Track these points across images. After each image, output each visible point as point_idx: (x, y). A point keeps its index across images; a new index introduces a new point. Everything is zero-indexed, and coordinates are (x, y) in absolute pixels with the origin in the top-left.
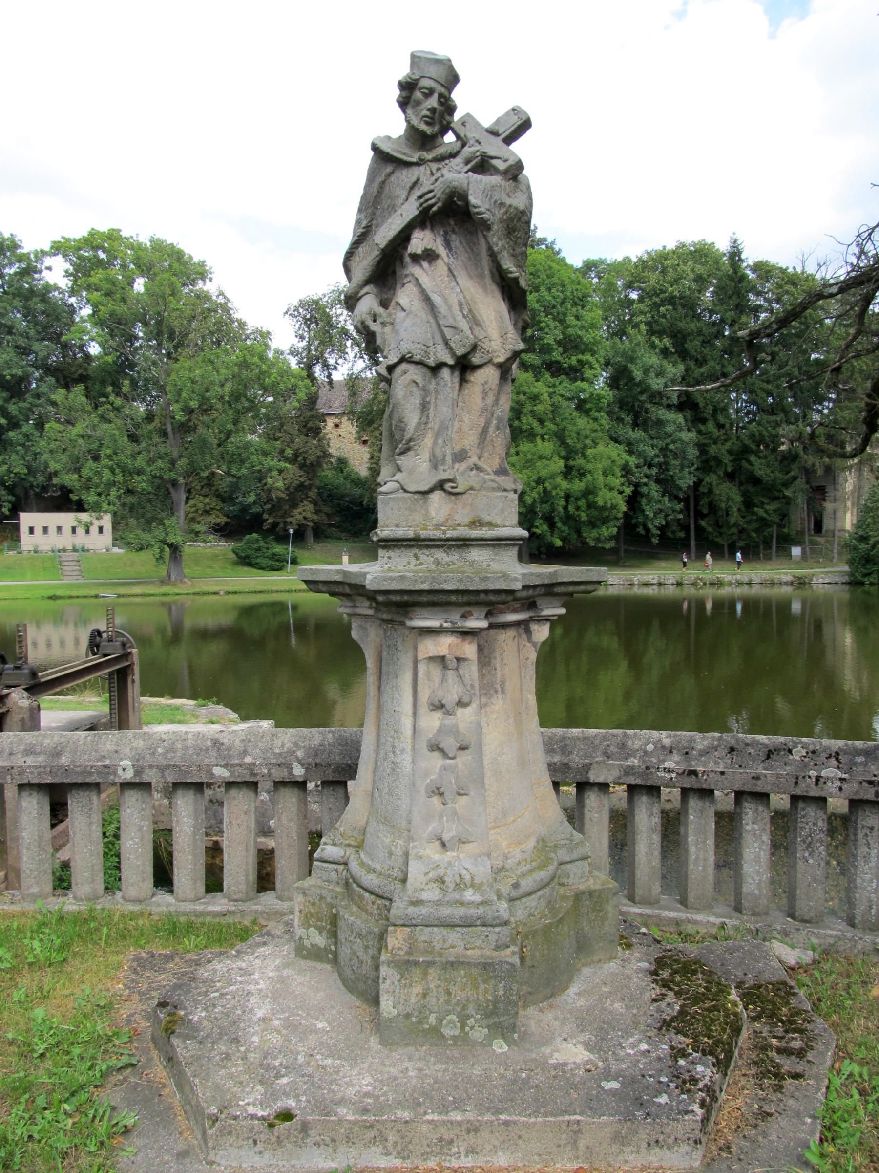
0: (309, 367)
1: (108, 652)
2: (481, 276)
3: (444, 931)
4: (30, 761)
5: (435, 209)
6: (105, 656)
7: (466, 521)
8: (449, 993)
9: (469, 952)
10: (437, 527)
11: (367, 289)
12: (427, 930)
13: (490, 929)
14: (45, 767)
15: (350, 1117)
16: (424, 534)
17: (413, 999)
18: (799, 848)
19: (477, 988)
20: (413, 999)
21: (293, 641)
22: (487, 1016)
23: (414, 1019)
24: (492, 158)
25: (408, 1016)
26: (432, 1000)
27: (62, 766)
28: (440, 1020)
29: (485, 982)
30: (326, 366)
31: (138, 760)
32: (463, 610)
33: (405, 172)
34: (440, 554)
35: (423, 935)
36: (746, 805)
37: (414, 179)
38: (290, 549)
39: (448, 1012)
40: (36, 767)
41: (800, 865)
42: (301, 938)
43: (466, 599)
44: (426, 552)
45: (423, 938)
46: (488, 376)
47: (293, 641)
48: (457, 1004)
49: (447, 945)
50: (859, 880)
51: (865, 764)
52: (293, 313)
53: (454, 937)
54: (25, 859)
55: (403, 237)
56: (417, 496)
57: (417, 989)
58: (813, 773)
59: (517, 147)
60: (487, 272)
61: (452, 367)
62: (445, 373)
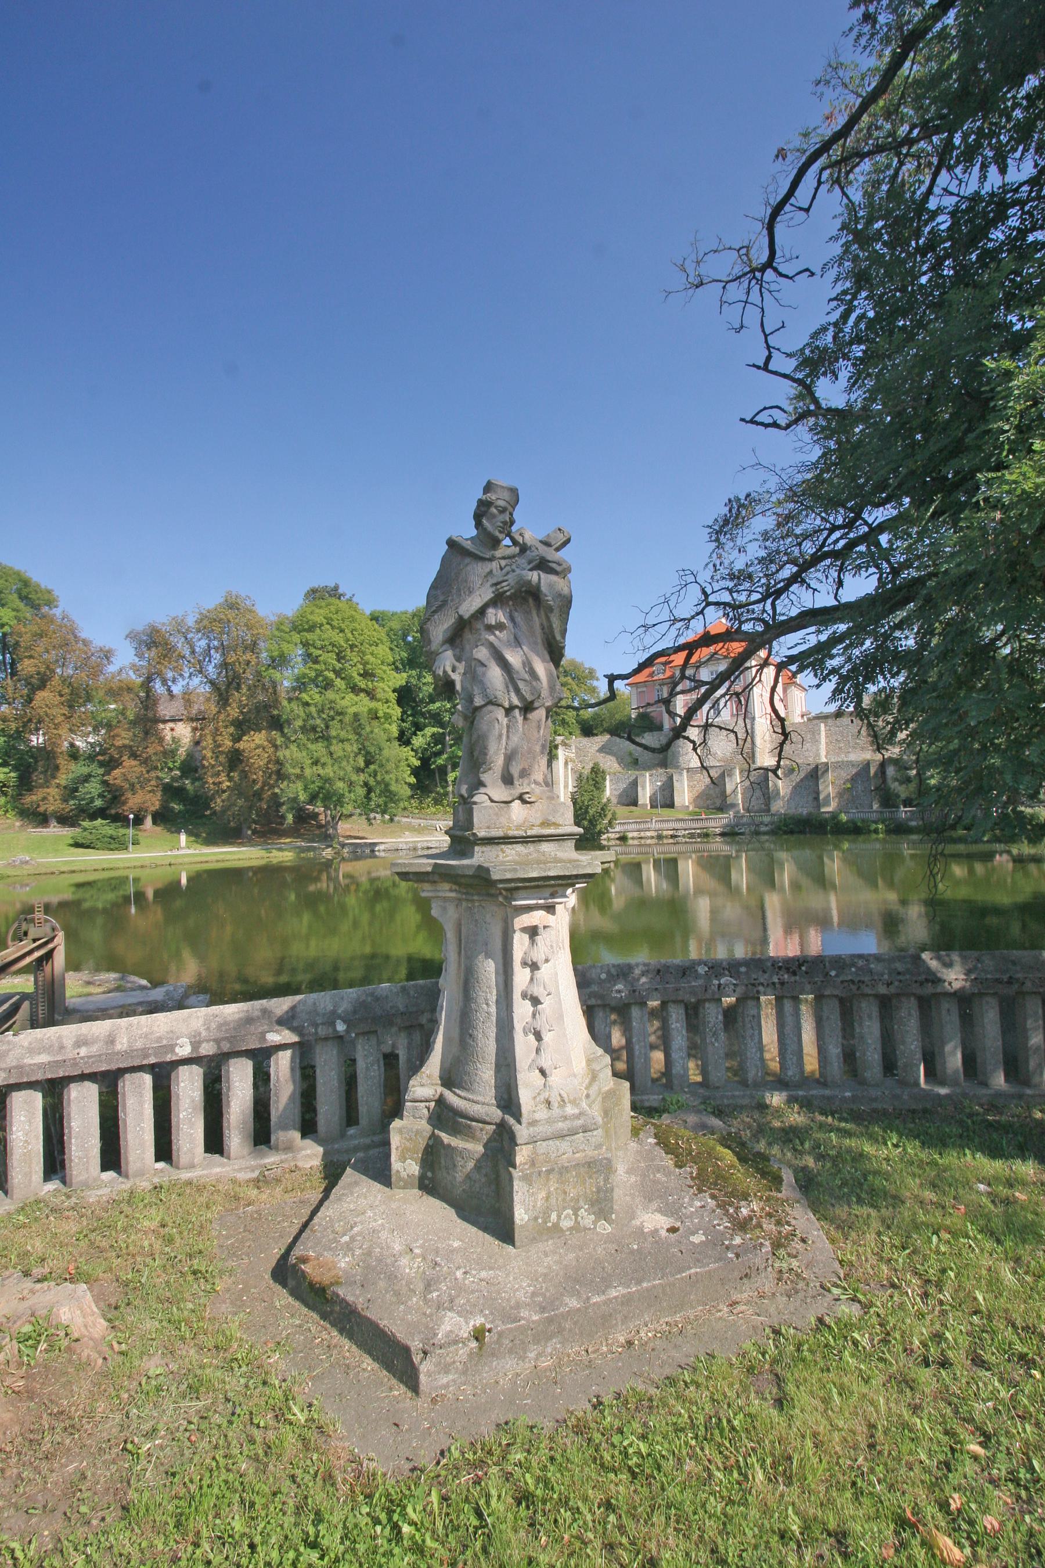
0: (149, 679)
1: (37, 936)
2: (536, 643)
3: (557, 1142)
4: (83, 1051)
5: (508, 593)
6: (34, 941)
7: (538, 822)
8: (565, 1193)
9: (577, 1155)
10: (518, 828)
11: (444, 648)
12: (544, 1144)
13: (590, 1133)
14: (100, 1055)
15: (535, 1318)
16: (511, 833)
17: (539, 1204)
18: (708, 1036)
19: (584, 1184)
20: (539, 1204)
21: (133, 910)
22: (592, 1205)
23: (540, 1221)
24: (549, 562)
25: (536, 1218)
26: (553, 1201)
27: (118, 1053)
28: (559, 1217)
29: (590, 1177)
30: (164, 682)
31: (195, 1037)
32: (551, 890)
33: (480, 564)
34: (519, 848)
35: (542, 1147)
36: (670, 1009)
37: (488, 570)
38: (131, 831)
39: (564, 1209)
40: (89, 1057)
41: (710, 1048)
42: (398, 1171)
43: (560, 882)
44: (510, 846)
45: (542, 1151)
46: (540, 714)
47: (133, 910)
48: (571, 1201)
49: (560, 1153)
50: (749, 1054)
51: (747, 973)
52: (132, 636)
53: (564, 1145)
54: (74, 1148)
55: (482, 612)
56: (502, 805)
57: (543, 1194)
58: (716, 982)
59: (563, 554)
60: (539, 641)
61: (520, 709)
62: (517, 711)
